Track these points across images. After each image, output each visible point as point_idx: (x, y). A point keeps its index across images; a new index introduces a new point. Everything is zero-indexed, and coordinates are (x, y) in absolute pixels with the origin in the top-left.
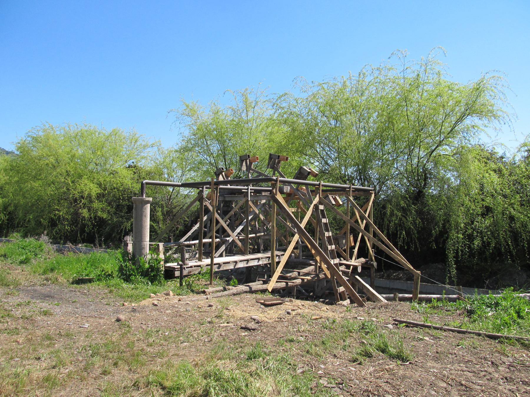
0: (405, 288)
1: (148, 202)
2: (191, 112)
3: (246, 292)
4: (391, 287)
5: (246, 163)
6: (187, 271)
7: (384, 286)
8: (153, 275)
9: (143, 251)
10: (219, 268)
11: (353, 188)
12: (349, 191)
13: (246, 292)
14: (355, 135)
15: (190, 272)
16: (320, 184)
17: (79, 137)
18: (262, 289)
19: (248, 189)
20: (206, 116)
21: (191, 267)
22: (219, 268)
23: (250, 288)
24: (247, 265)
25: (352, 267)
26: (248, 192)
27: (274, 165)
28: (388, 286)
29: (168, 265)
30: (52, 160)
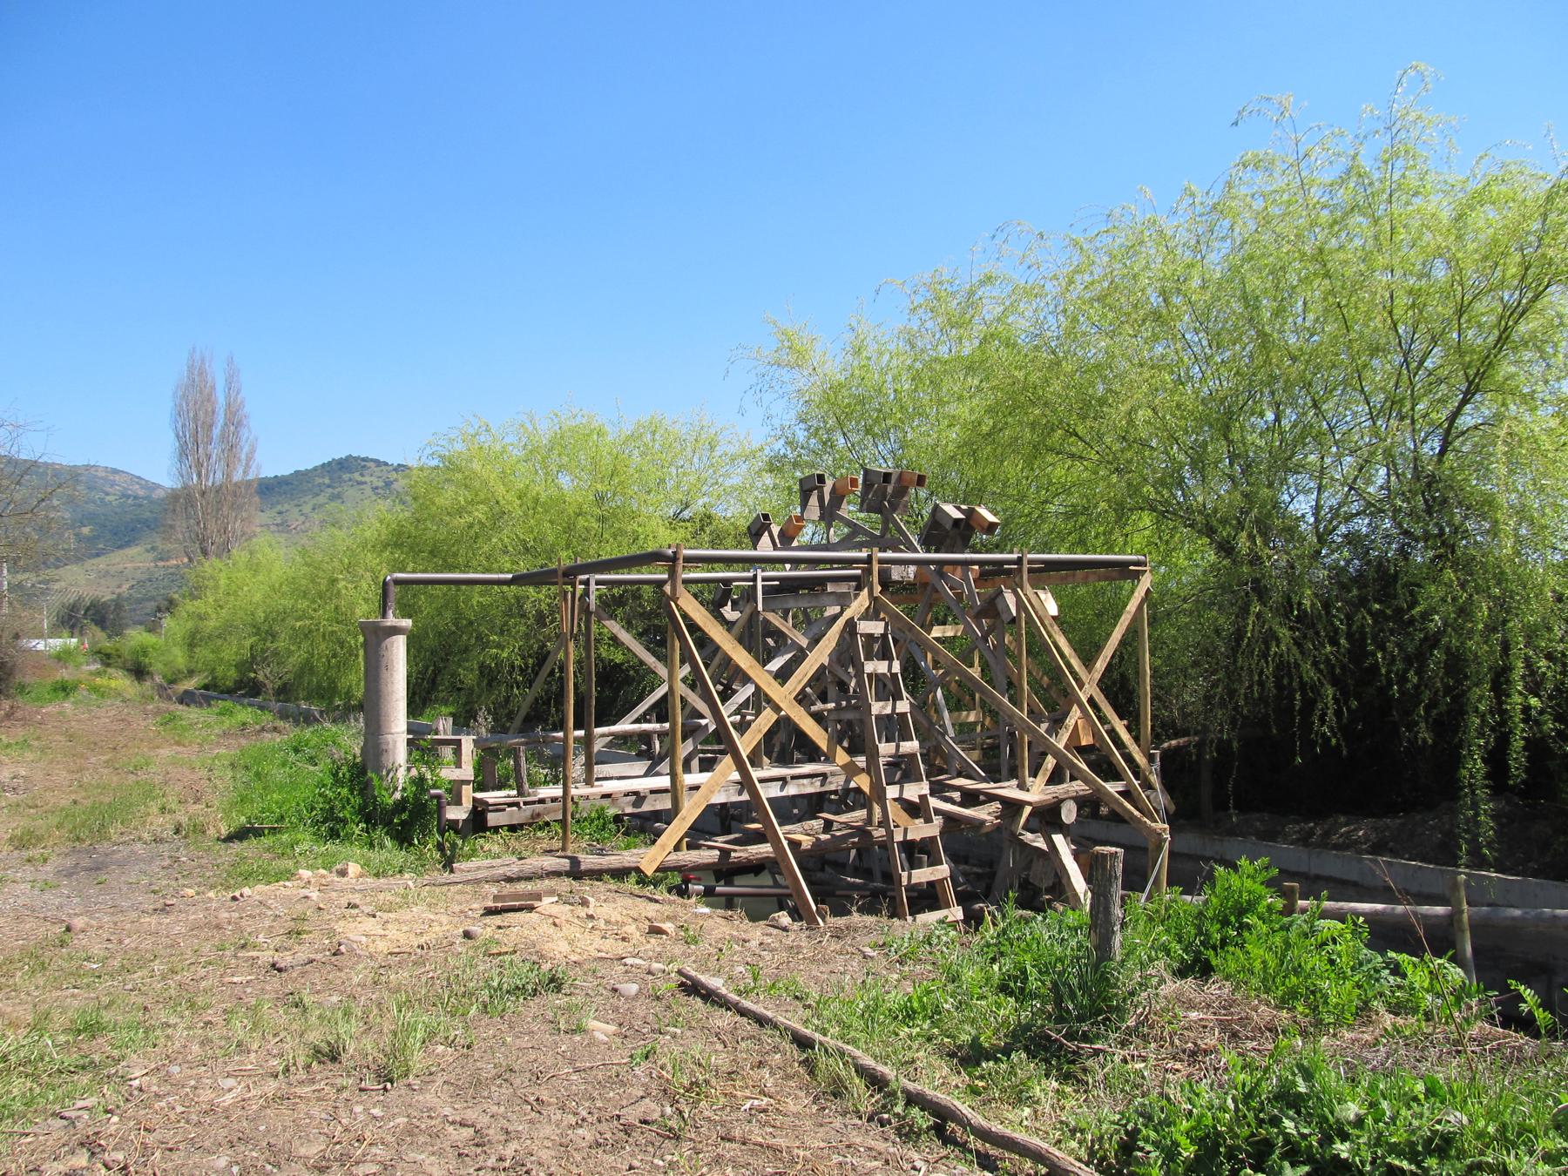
0: (1354, 877)
1: (395, 631)
2: (793, 355)
3: (557, 874)
4: (1314, 871)
5: (821, 499)
6: (528, 813)
7: (1293, 869)
8: (409, 822)
9: (383, 759)
10: (637, 804)
11: (1030, 562)
12: (1020, 570)
13: (557, 874)
14: (1160, 379)
15: (539, 815)
16: (870, 557)
17: (563, 447)
18: (618, 865)
19: (754, 579)
20: (832, 363)
21: (542, 801)
22: (637, 804)
23: (575, 861)
24: (784, 793)
25: (1028, 810)
26: (755, 587)
27: (881, 502)
28: (1303, 869)
29: (479, 795)
30: (480, 513)
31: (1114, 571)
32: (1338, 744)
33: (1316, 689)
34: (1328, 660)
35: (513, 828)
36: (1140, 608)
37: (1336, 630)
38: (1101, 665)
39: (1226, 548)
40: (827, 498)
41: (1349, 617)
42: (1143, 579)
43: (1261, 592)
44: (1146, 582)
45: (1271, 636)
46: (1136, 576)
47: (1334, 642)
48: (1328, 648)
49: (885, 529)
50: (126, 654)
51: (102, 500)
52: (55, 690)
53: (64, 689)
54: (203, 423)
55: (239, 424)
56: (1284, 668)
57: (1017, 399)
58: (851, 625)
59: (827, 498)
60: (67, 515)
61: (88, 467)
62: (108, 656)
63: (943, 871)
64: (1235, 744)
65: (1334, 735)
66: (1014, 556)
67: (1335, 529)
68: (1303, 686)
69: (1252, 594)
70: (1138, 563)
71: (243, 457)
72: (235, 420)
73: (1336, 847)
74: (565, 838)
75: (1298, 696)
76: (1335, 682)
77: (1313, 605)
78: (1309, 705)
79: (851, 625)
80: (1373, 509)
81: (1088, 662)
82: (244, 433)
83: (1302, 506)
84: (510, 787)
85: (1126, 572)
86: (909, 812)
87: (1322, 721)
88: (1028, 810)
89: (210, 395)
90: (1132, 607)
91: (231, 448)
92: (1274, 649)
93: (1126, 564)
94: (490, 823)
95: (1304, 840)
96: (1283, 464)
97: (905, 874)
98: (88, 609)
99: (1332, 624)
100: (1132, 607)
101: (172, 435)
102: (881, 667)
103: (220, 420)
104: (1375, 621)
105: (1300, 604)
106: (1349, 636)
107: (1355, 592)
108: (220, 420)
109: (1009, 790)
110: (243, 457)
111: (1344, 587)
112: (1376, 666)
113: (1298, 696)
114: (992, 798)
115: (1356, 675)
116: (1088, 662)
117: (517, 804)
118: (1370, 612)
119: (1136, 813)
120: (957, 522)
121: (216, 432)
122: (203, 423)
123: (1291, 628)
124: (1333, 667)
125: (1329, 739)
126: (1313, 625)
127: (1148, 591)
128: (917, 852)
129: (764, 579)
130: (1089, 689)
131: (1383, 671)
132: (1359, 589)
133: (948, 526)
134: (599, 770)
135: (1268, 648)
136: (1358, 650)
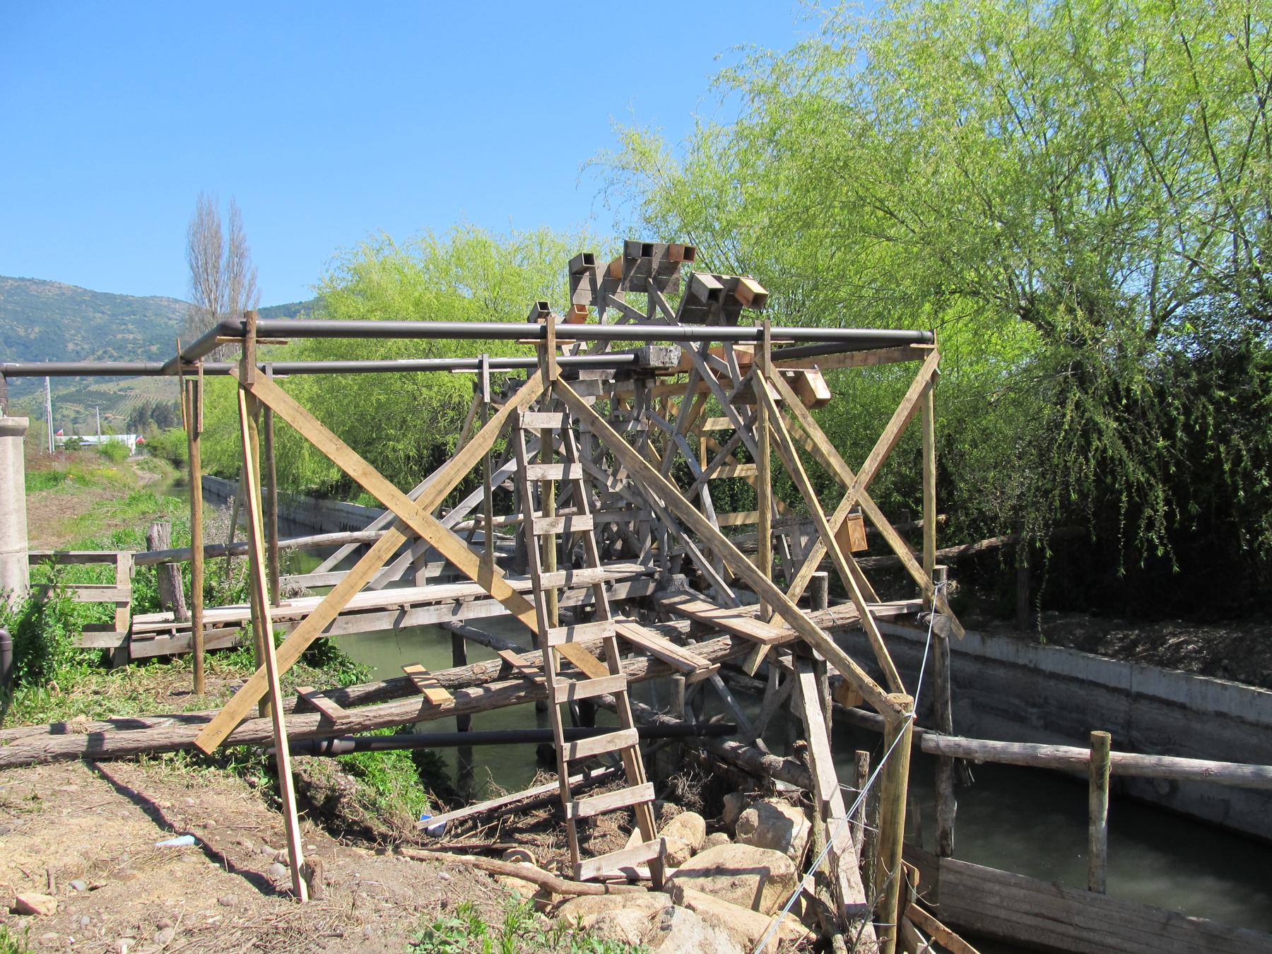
0: (1181, 698)
4: (1135, 689)
5: (593, 282)
11: (774, 337)
16: (544, 329)
20: (672, 166)
25: (764, 649)
28: (1124, 684)
31: (895, 352)
32: (1166, 553)
33: (1143, 489)
34: (1159, 455)
35: (165, 659)
36: (923, 395)
37: (1172, 422)
38: (870, 465)
39: (1048, 330)
40: (599, 281)
41: (1187, 411)
42: (928, 359)
43: (1083, 378)
44: (932, 363)
45: (1090, 430)
46: (921, 355)
47: (1168, 434)
48: (1161, 443)
49: (652, 310)
50: (169, 447)
51: (166, 324)
52: (49, 480)
53: (55, 479)
54: (212, 255)
55: (242, 256)
56: (1106, 465)
57: (824, 174)
58: (513, 417)
59: (599, 281)
60: (139, 337)
61: (153, 298)
62: (155, 448)
63: (630, 736)
64: (1049, 553)
65: (1162, 544)
66: (754, 330)
67: (1173, 310)
68: (1129, 485)
69: (1071, 380)
70: (921, 340)
71: (246, 283)
72: (238, 252)
73: (1162, 663)
74: (196, 679)
75: (1124, 498)
76: (1167, 479)
77: (1144, 391)
78: (1135, 511)
79: (513, 417)
80: (1218, 286)
81: (855, 463)
82: (246, 263)
83: (1134, 285)
84: (168, 609)
85: (906, 350)
86: (585, 658)
87: (1150, 525)
88: (764, 649)
89: (217, 233)
90: (913, 393)
91: (236, 277)
92: (1096, 443)
93: (907, 341)
94: (134, 655)
95: (1127, 652)
96: (1115, 233)
97: (567, 746)
98: (154, 411)
99: (1167, 414)
100: (913, 393)
101: (188, 268)
102: (554, 472)
103: (226, 254)
104: (1218, 410)
105: (1128, 390)
106: (1187, 428)
107: (1194, 377)
108: (226, 254)
109: (747, 624)
110: (246, 283)
111: (1183, 373)
112: (1218, 461)
113: (1124, 498)
114: (725, 630)
115: (1195, 475)
116: (855, 463)
117: (169, 632)
118: (1211, 400)
119: (868, 680)
120: (713, 293)
121: (223, 263)
122: (212, 255)
123: (1117, 419)
124: (1167, 465)
125: (1156, 548)
126: (1144, 415)
127: (934, 374)
128: (589, 716)
129: (492, 366)
130: (857, 491)
131: (1227, 467)
132: (1198, 374)
133: (704, 298)
134: (288, 581)
135: (1089, 443)
136: (1197, 442)
